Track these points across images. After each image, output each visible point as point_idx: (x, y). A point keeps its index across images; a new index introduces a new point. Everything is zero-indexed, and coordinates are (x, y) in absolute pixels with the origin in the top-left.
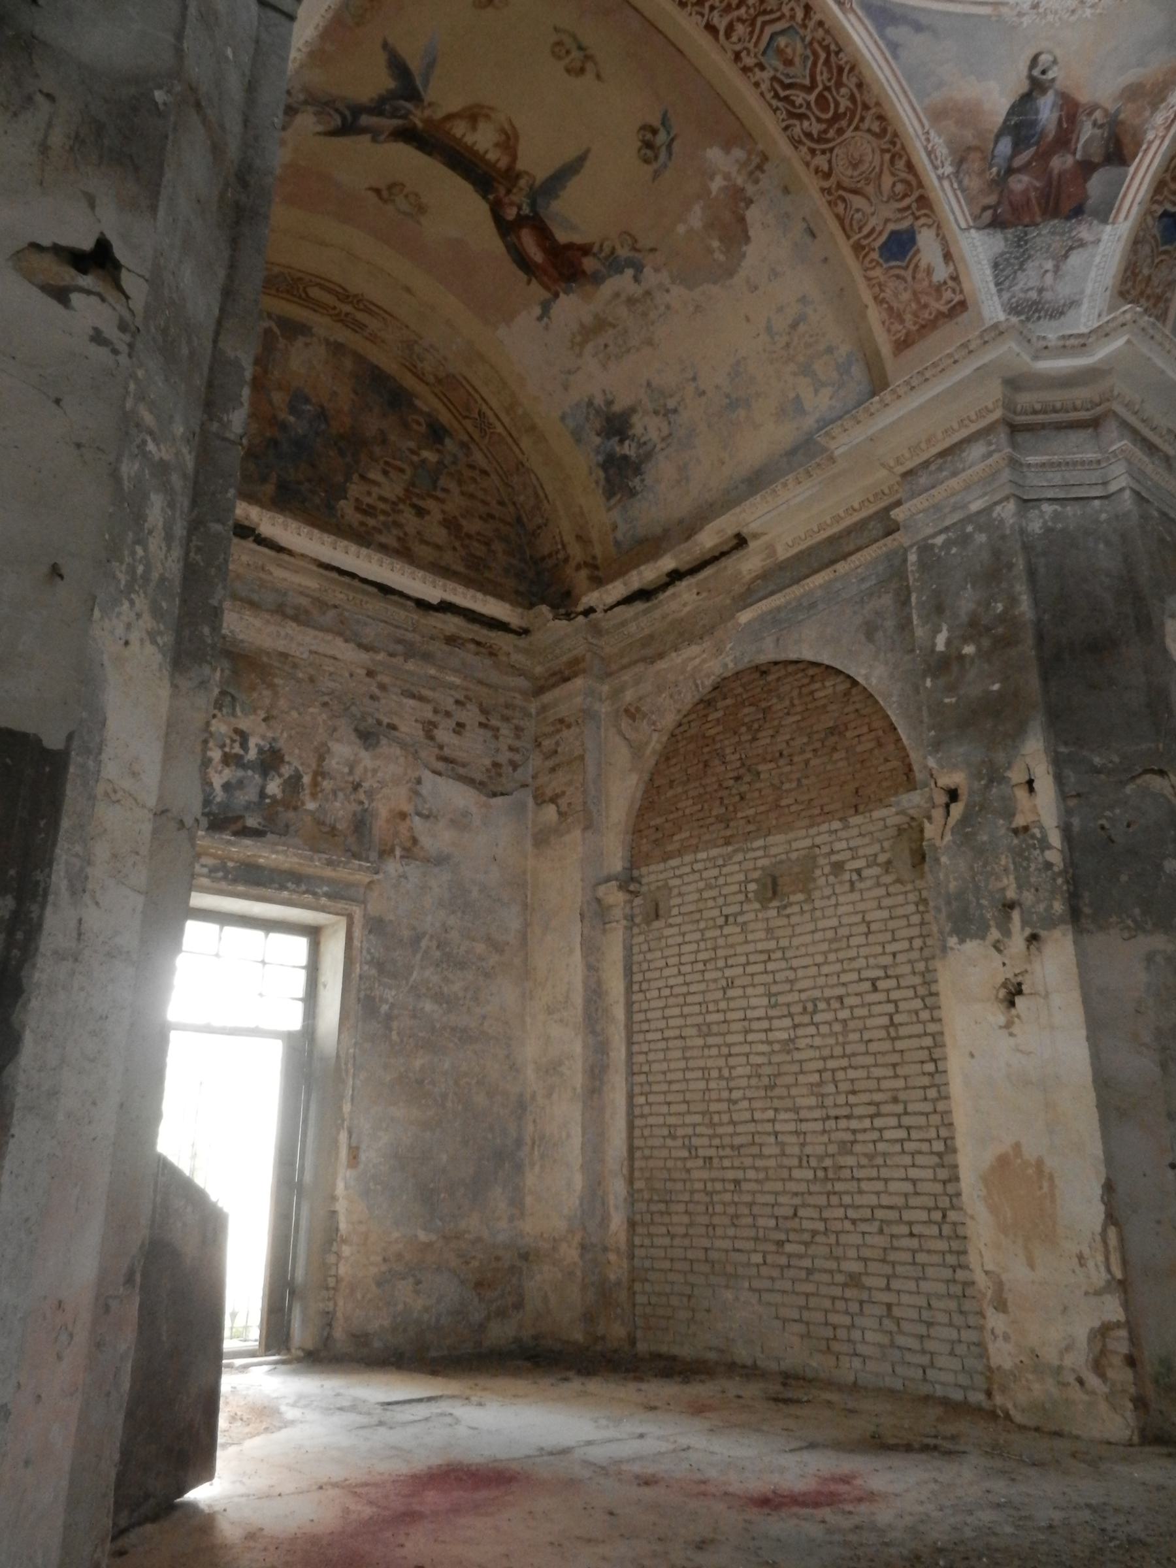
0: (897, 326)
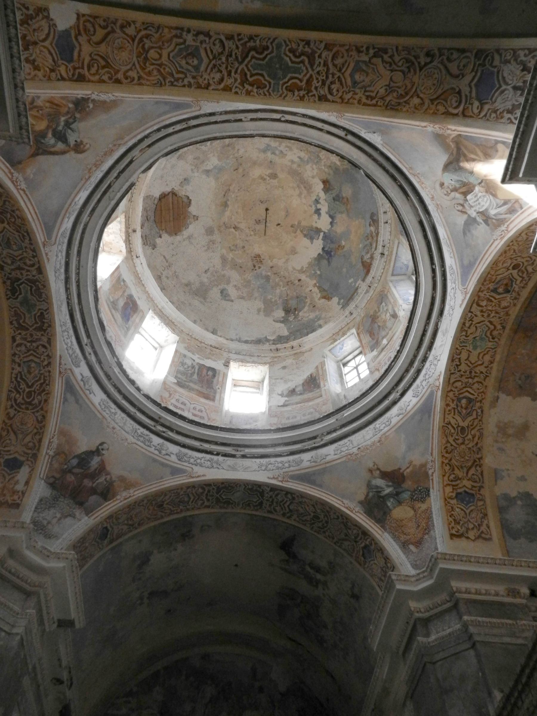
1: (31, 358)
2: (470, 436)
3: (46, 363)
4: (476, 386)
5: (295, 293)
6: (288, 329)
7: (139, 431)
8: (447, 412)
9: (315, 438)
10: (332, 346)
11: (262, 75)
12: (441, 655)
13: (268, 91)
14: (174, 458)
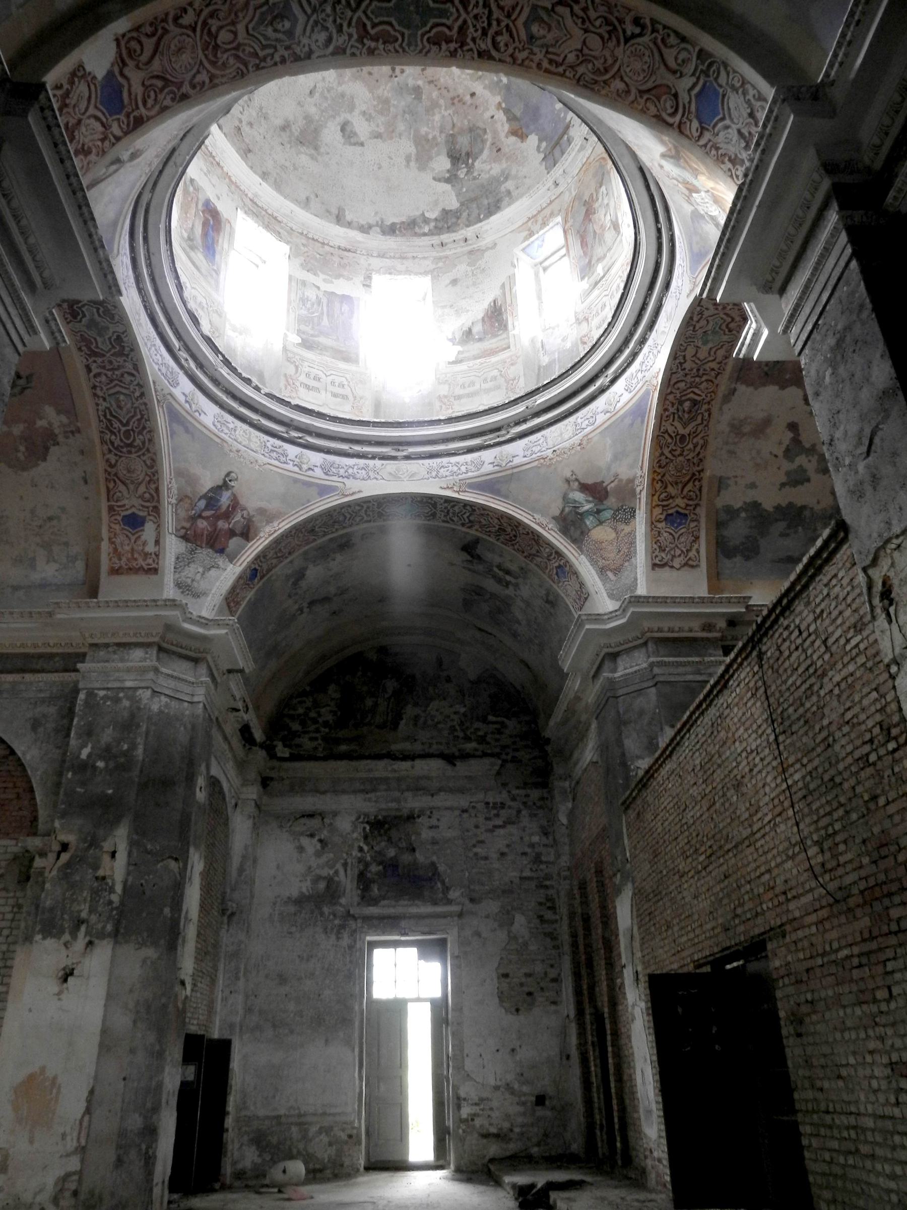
0: (115, 560)
1: (117, 389)
2: (691, 446)
3: (137, 394)
4: (704, 385)
5: (466, 122)
6: (458, 195)
7: (268, 444)
8: (664, 418)
9: (498, 429)
10: (527, 243)
11: (390, 24)
12: (624, 691)
13: (401, 46)
14: (318, 473)
